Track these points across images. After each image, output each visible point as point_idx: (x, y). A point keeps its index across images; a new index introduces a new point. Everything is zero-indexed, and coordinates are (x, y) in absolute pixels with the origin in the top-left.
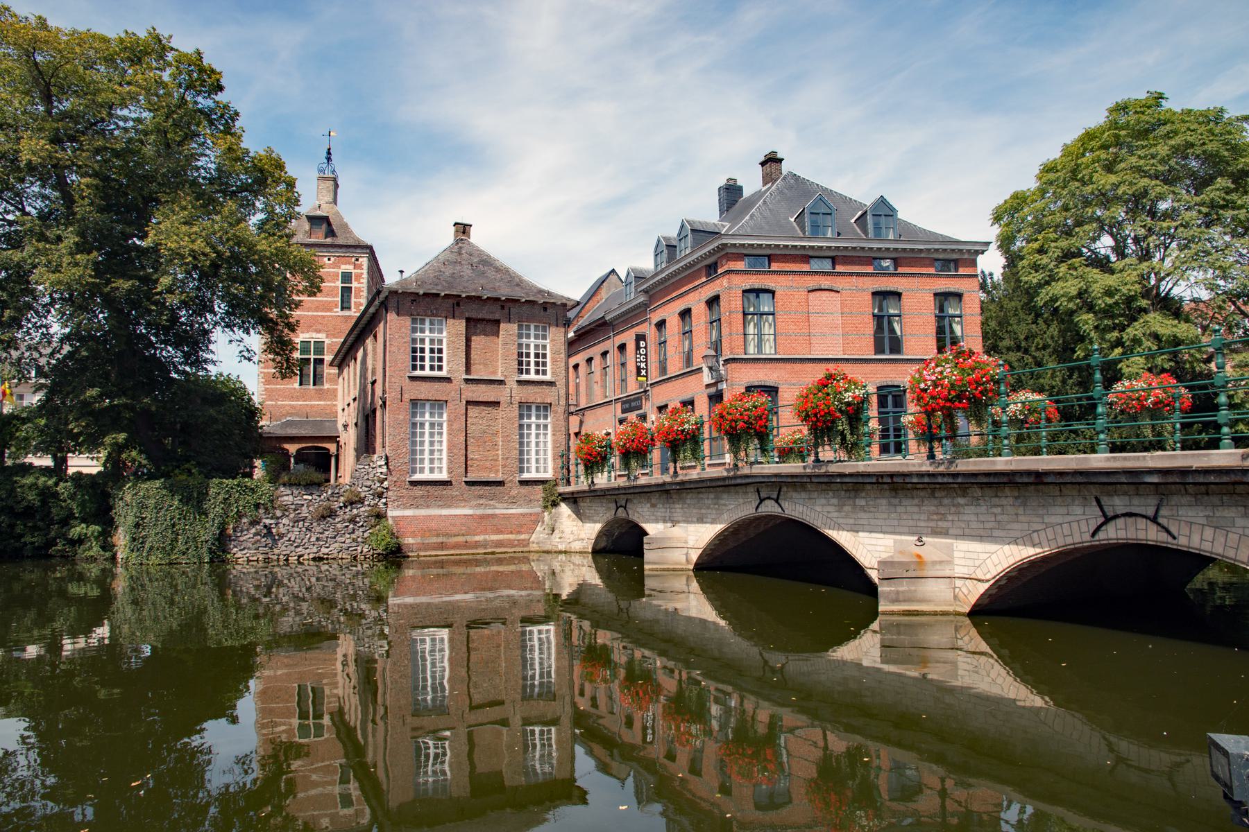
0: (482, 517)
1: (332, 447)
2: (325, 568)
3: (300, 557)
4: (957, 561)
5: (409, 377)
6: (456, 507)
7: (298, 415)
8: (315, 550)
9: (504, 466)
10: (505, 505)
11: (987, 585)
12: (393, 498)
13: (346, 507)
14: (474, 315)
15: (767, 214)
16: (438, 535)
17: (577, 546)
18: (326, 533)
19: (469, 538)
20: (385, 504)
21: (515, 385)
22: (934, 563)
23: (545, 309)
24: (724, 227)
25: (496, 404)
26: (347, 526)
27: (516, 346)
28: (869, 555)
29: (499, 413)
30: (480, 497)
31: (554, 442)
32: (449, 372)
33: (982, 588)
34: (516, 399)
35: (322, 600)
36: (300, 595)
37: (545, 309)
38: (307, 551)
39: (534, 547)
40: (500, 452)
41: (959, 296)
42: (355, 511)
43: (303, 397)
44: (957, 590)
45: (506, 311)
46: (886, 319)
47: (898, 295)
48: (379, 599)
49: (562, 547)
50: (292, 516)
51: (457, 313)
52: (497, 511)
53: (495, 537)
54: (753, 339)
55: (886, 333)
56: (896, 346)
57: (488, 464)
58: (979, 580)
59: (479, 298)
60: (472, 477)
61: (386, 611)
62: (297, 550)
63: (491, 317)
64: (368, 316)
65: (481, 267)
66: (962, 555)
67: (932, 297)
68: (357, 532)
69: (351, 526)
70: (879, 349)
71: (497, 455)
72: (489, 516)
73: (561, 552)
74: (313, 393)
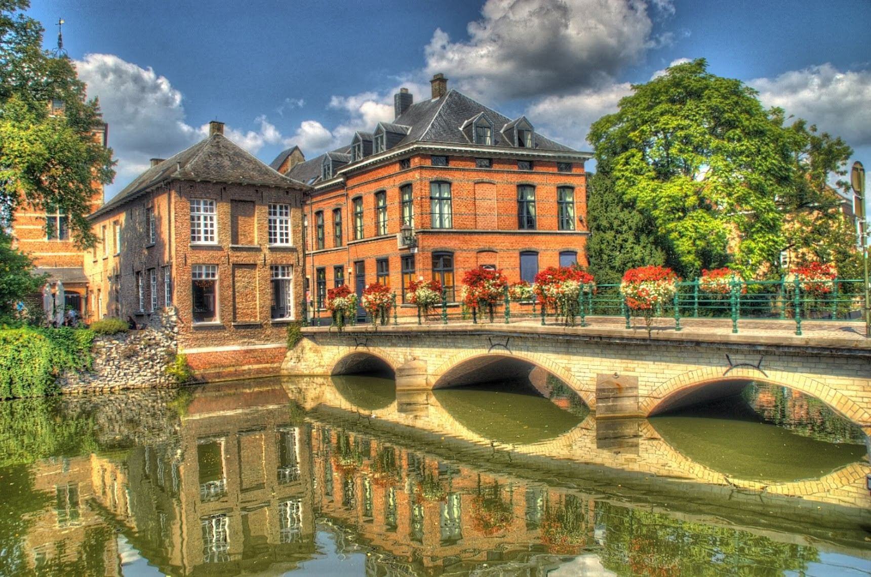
0: (247, 352)
1: (82, 292)
2: (131, 395)
3: (112, 388)
4: (640, 387)
5: (191, 246)
6: (228, 345)
7: (48, 265)
8: (124, 383)
9: (261, 313)
10: (262, 342)
11: (659, 401)
12: (181, 340)
13: (146, 348)
14: (236, 197)
15: (443, 124)
16: (216, 367)
17: (319, 371)
18: (132, 369)
19: (238, 368)
20: (176, 345)
21: (267, 252)
22: (627, 388)
23: (287, 193)
24: (408, 129)
25: (253, 266)
26: (146, 364)
27: (267, 222)
28: (579, 383)
29: (257, 273)
30: (244, 337)
31: (296, 293)
32: (219, 242)
33: (657, 402)
34: (268, 262)
35: (131, 421)
36: (113, 417)
37: (287, 193)
38: (118, 384)
39: (285, 372)
40: (258, 302)
41: (572, 188)
42: (153, 352)
43: (51, 249)
44: (640, 404)
45: (260, 194)
46: (525, 204)
47: (533, 187)
48: (174, 416)
49: (306, 372)
50: (104, 357)
51: (223, 196)
52: (257, 347)
53: (256, 366)
54: (448, 217)
55: (525, 214)
56: (531, 223)
57: (249, 311)
58: (655, 398)
59: (240, 184)
60: (240, 320)
61: (179, 425)
62: (110, 383)
63: (249, 199)
64: (143, 192)
65: (236, 159)
66: (644, 383)
67: (516, 188)
68: (155, 368)
69: (151, 363)
70: (521, 226)
71: (256, 304)
72: (251, 350)
73: (306, 376)
74: (60, 245)
